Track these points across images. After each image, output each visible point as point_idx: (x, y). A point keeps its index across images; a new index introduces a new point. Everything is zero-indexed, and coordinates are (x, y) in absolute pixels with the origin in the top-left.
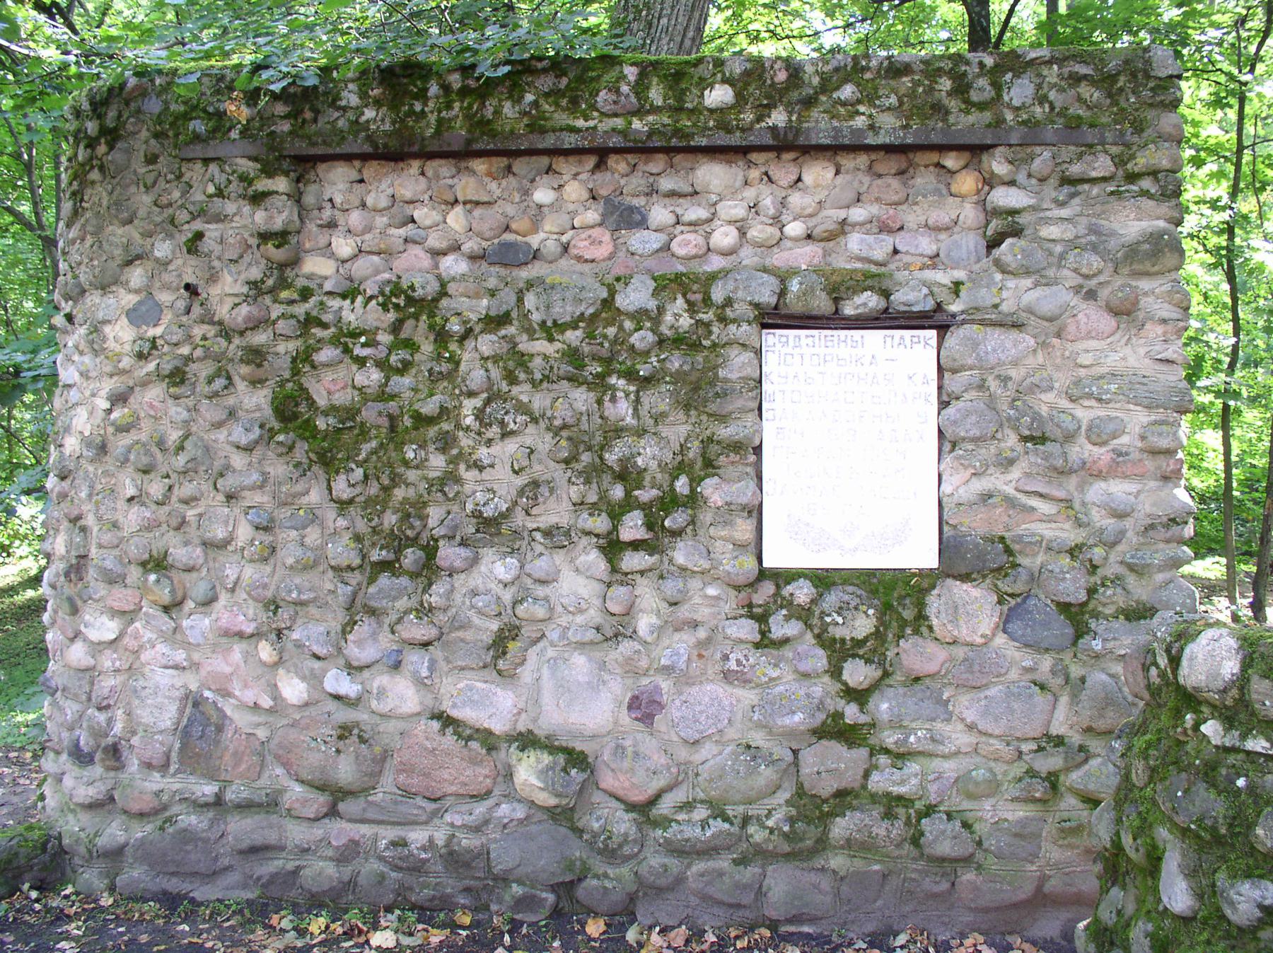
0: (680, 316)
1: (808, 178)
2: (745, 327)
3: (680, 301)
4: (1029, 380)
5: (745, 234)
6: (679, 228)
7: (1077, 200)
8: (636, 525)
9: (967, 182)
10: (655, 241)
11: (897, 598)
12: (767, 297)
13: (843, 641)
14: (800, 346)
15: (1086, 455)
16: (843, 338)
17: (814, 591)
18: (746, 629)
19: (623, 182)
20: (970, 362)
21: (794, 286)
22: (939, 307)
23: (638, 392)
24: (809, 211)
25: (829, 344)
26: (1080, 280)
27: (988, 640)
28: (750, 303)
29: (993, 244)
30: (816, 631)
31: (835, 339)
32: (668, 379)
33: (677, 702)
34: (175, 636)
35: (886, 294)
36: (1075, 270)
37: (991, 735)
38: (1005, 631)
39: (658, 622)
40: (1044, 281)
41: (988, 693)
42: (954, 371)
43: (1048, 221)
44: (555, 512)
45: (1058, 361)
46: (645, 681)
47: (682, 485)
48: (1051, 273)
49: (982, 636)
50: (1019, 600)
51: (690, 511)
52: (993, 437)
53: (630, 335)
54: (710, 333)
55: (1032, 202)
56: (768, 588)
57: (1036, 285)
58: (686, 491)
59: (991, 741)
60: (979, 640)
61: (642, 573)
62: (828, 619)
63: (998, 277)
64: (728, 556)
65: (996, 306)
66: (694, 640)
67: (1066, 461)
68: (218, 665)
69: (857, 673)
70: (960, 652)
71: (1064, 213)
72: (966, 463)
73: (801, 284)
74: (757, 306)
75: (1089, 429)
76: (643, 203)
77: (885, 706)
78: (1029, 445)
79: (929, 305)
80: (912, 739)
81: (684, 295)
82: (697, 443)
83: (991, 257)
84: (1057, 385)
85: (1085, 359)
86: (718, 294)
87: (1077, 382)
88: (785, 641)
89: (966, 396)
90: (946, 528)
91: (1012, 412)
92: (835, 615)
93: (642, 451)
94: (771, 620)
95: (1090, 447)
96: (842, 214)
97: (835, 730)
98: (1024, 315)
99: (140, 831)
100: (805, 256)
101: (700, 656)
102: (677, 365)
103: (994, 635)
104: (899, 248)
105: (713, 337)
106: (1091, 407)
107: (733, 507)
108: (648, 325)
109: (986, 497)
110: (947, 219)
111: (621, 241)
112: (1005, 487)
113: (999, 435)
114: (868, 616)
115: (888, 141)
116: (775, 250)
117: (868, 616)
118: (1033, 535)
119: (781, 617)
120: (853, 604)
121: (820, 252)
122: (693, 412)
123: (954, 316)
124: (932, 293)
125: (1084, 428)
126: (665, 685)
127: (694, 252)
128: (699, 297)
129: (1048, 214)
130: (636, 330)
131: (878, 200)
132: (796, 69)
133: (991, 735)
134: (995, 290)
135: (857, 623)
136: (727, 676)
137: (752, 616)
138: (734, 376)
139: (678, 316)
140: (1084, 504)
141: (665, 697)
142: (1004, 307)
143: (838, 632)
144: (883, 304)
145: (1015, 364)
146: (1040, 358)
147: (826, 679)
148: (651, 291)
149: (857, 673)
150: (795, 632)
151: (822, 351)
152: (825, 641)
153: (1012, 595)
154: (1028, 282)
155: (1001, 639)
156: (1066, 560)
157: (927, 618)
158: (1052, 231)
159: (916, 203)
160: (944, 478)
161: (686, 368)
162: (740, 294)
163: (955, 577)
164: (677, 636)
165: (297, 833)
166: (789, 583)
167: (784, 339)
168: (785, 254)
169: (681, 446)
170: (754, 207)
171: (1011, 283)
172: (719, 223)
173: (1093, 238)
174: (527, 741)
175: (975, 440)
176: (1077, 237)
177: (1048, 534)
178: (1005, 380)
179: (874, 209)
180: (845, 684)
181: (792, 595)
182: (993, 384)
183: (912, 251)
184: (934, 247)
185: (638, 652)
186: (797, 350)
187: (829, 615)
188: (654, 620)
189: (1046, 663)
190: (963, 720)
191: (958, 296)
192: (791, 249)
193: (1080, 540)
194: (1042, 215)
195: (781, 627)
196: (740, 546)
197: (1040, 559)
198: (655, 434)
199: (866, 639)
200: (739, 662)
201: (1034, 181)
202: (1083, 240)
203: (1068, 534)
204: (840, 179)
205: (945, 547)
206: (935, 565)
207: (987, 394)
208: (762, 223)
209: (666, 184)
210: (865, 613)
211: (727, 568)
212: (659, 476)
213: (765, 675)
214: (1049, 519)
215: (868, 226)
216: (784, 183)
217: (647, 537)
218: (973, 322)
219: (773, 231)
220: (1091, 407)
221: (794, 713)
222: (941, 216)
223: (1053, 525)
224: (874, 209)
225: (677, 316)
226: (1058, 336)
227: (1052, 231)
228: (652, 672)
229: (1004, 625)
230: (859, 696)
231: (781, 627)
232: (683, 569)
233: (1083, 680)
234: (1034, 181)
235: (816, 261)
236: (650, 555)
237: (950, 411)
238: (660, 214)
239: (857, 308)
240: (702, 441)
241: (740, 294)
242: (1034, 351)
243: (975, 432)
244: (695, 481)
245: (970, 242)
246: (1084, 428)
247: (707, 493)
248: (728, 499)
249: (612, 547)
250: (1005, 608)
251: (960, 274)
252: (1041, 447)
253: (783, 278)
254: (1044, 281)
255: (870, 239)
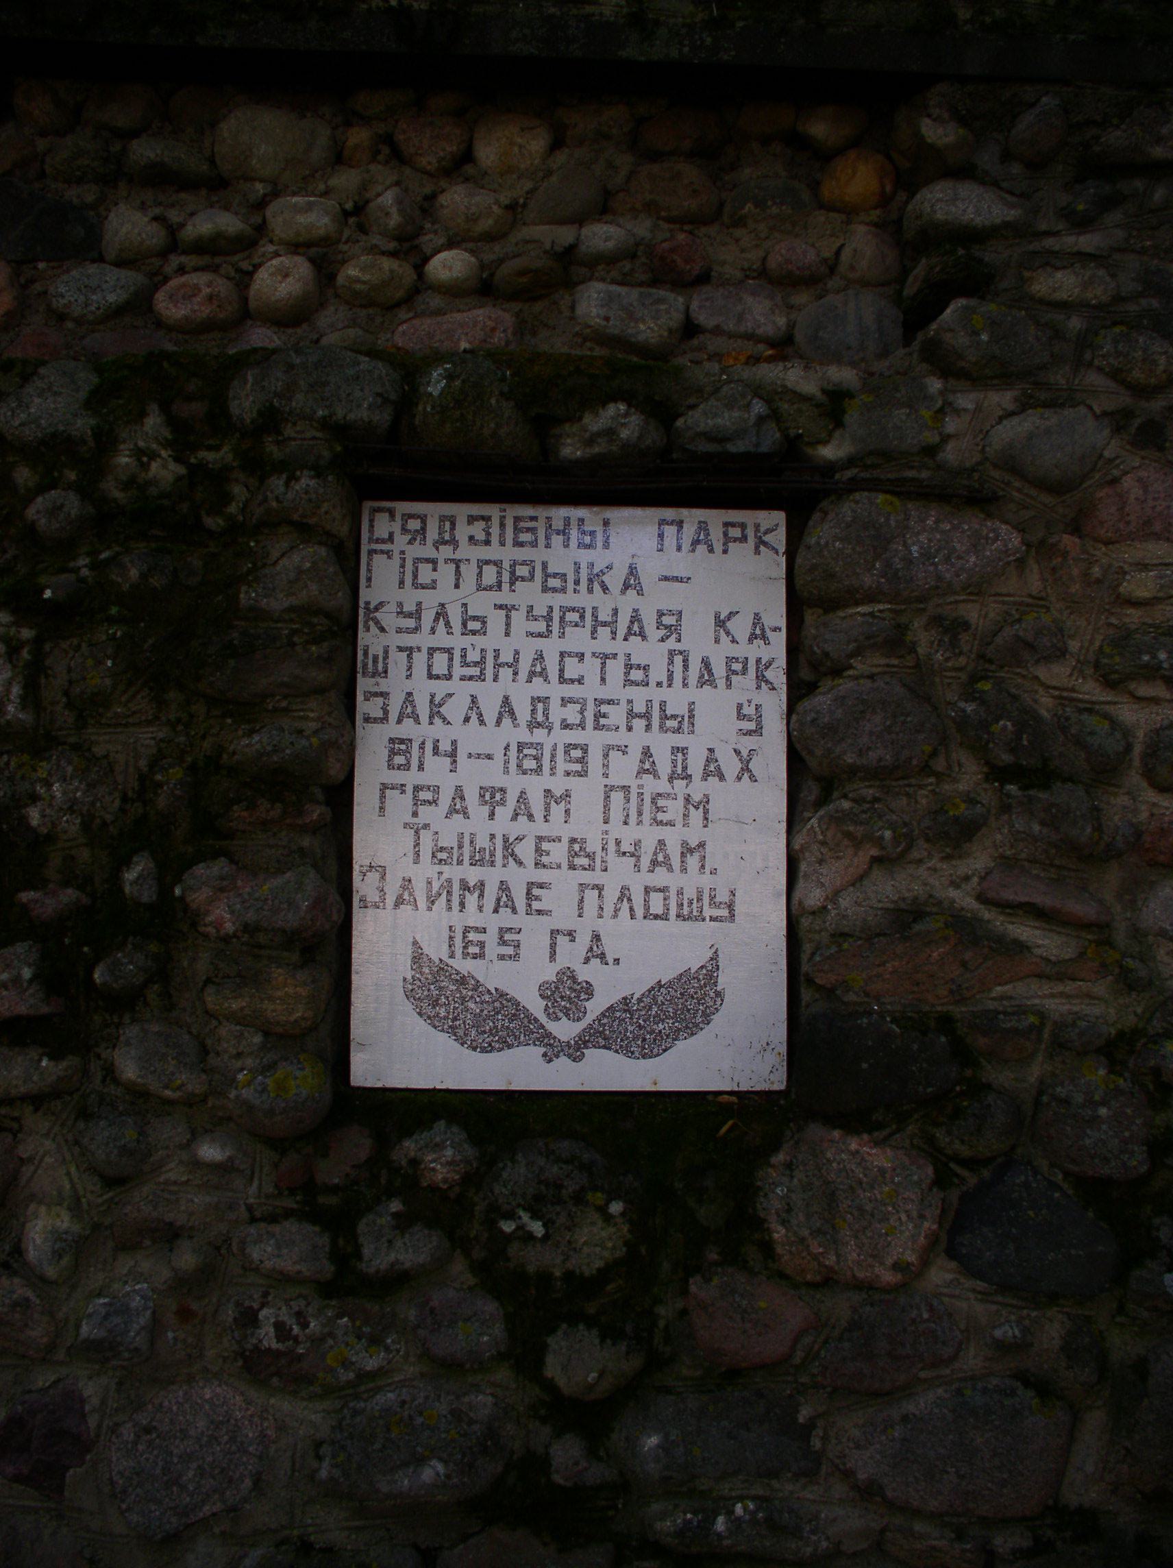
0: (153, 456)
1: (488, 153)
2: (306, 481)
3: (153, 421)
4: (1008, 632)
5: (332, 277)
6: (175, 260)
7: (1115, 217)
8: (17, 980)
9: (858, 179)
10: (110, 286)
12: (363, 406)
13: (544, 1278)
14: (454, 542)
15: (1144, 816)
16: (558, 524)
17: (470, 1151)
18: (288, 1249)
19: (42, 144)
20: (868, 580)
21: (436, 384)
22: (792, 448)
23: (38, 641)
24: (486, 224)
25: (525, 537)
26: (1125, 399)
27: (910, 1274)
28: (325, 424)
29: (917, 315)
30: (478, 1254)
31: (541, 526)
32: (114, 610)
33: (127, 1432)
35: (662, 412)
36: (1116, 375)
37: (917, 1513)
38: (952, 1253)
39: (76, 1228)
40: (1043, 396)
41: (910, 1407)
42: (831, 604)
43: (1051, 260)
45: (1075, 588)
46: (43, 1379)
47: (137, 875)
48: (1059, 378)
49: (896, 1267)
50: (986, 1173)
51: (153, 947)
52: (926, 769)
53: (29, 500)
54: (226, 498)
55: (1012, 214)
56: (356, 1145)
57: (1024, 406)
58: (148, 895)
59: (918, 1527)
60: (888, 1277)
61: (37, 1100)
62: (508, 1227)
63: (935, 385)
64: (249, 1062)
65: (930, 451)
66: (166, 1274)
67: (1099, 828)
69: (580, 1361)
70: (841, 1307)
71: (1088, 242)
72: (859, 831)
73: (450, 377)
74: (337, 430)
75: (1152, 751)
76: (90, 199)
77: (653, 1441)
78: (1012, 788)
79: (770, 439)
80: (720, 1524)
81: (165, 407)
82: (177, 773)
83: (916, 345)
84: (1074, 645)
85: (1141, 586)
86: (245, 402)
87: (1122, 640)
88: (396, 1281)
89: (860, 666)
90: (806, 995)
91: (970, 708)
92: (525, 1217)
93: (40, 790)
94: (362, 1227)
95: (1151, 795)
96: (565, 235)
98: (996, 474)
99: (178, 1094)
100: (474, 327)
101: (185, 1314)
102: (134, 573)
103: (925, 1263)
104: (702, 318)
105: (233, 509)
106: (1155, 701)
107: (262, 938)
108: (72, 476)
109: (906, 917)
110: (811, 256)
111: (38, 287)
112: (953, 893)
113: (940, 764)
114: (608, 1218)
115: (674, 54)
116: (403, 314)
117: (608, 1218)
118: (1021, 1011)
119: (385, 1220)
120: (571, 1187)
121: (508, 319)
122: (172, 695)
123: (830, 468)
124: (775, 415)
125: (1138, 749)
126: (92, 1389)
127: (205, 311)
128: (197, 409)
129: (1049, 242)
130: (41, 489)
131: (650, 208)
133: (917, 1513)
134: (926, 414)
135: (582, 1236)
136: (256, 1367)
137: (310, 1213)
138: (277, 603)
139: (148, 456)
140: (1137, 933)
141: (92, 1422)
142: (950, 454)
143: (534, 1259)
144: (654, 437)
145: (977, 589)
146: (1034, 581)
147: (503, 1374)
148: (83, 395)
150: (422, 1258)
151: (508, 554)
152: (497, 1275)
153: (972, 1164)
154: (1004, 399)
155: (941, 1274)
156: (1097, 1074)
157: (759, 1224)
158: (1062, 283)
159: (740, 222)
160: (803, 867)
161: (156, 582)
162: (299, 401)
163: (832, 1121)
164: (125, 1264)
166: (409, 1134)
167: (414, 525)
168: (426, 324)
169: (142, 778)
170: (356, 214)
171: (966, 401)
172: (271, 248)
173: (1155, 303)
175: (878, 774)
176: (1118, 299)
177: (1057, 1007)
178: (952, 629)
179: (642, 228)
180: (550, 1386)
181: (414, 1162)
182: (923, 638)
183: (731, 326)
184: (782, 321)
185: (24, 1304)
186: (446, 551)
187: (511, 1216)
188: (65, 1221)
189: (1052, 1330)
190: (848, 1474)
191: (839, 424)
192: (439, 312)
193: (1130, 1021)
194: (1035, 246)
195: (388, 1248)
196: (282, 1040)
197: (1036, 1071)
198: (76, 747)
199: (604, 1275)
200: (282, 1331)
201: (1016, 169)
202: (1132, 307)
203: (1097, 1006)
204: (561, 157)
206: (778, 1082)
207: (910, 661)
208: (373, 250)
209: (145, 151)
210: (603, 1210)
211: (246, 1093)
212: (85, 854)
213: (346, 1364)
214: (1057, 972)
215: (627, 266)
216: (428, 161)
217: (45, 1010)
218: (874, 485)
219: (405, 271)
220: (1155, 701)
221: (421, 1461)
222: (797, 251)
223: (1069, 987)
224: (642, 228)
225: (143, 456)
226: (1076, 529)
227: (1062, 283)
228: (61, 1355)
229: (951, 1240)
230: (589, 1417)
231: (388, 1248)
232: (138, 1094)
233: (1141, 1368)
234: (1016, 169)
235: (498, 339)
236: (55, 1057)
237: (821, 702)
238: (129, 224)
239: (590, 442)
240: (193, 768)
241: (299, 401)
242: (1021, 563)
243: (880, 754)
244: (171, 869)
245: (862, 313)
246: (1138, 749)
247: (198, 898)
248: (251, 916)
250: (954, 1196)
251: (843, 375)
252: (1043, 795)
253: (409, 369)
254: (1043, 396)
255: (631, 295)
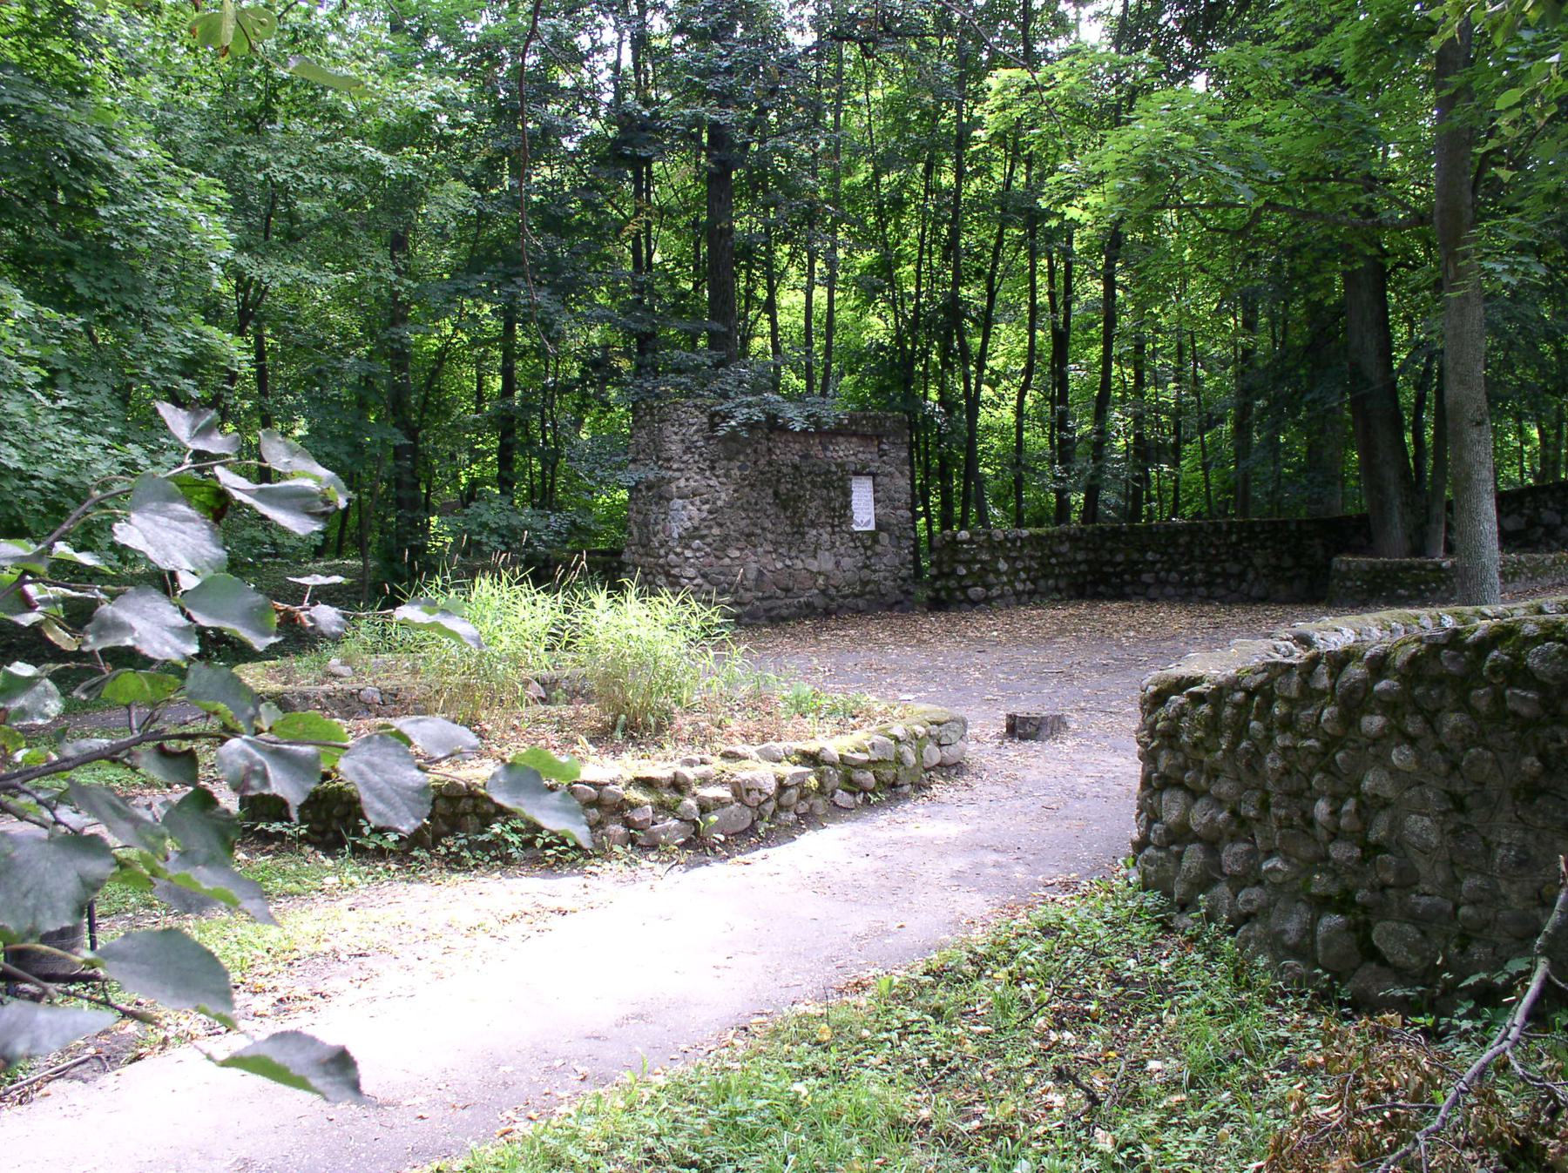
11: (873, 536)
34: (755, 554)
44: (823, 519)
68: (764, 560)
97: (866, 567)
132: (602, 161)
149: (869, 553)
165: (779, 603)
174: (820, 573)
205: (877, 524)
249: (833, 526)
